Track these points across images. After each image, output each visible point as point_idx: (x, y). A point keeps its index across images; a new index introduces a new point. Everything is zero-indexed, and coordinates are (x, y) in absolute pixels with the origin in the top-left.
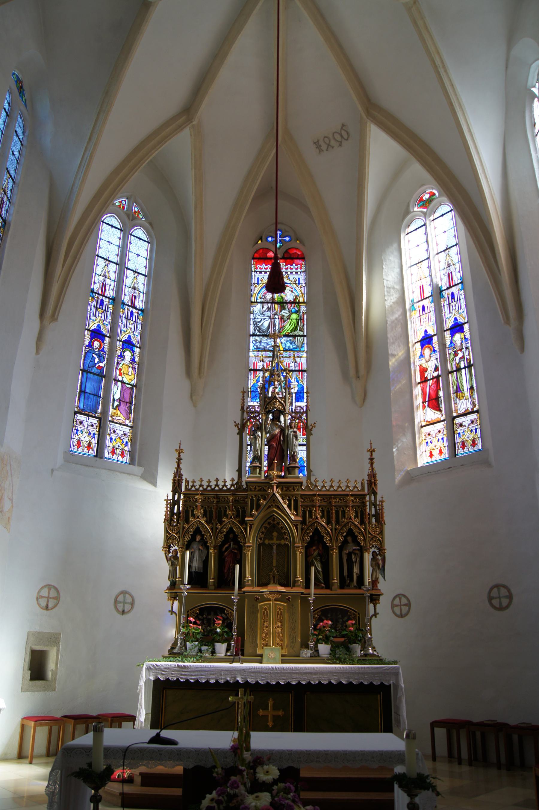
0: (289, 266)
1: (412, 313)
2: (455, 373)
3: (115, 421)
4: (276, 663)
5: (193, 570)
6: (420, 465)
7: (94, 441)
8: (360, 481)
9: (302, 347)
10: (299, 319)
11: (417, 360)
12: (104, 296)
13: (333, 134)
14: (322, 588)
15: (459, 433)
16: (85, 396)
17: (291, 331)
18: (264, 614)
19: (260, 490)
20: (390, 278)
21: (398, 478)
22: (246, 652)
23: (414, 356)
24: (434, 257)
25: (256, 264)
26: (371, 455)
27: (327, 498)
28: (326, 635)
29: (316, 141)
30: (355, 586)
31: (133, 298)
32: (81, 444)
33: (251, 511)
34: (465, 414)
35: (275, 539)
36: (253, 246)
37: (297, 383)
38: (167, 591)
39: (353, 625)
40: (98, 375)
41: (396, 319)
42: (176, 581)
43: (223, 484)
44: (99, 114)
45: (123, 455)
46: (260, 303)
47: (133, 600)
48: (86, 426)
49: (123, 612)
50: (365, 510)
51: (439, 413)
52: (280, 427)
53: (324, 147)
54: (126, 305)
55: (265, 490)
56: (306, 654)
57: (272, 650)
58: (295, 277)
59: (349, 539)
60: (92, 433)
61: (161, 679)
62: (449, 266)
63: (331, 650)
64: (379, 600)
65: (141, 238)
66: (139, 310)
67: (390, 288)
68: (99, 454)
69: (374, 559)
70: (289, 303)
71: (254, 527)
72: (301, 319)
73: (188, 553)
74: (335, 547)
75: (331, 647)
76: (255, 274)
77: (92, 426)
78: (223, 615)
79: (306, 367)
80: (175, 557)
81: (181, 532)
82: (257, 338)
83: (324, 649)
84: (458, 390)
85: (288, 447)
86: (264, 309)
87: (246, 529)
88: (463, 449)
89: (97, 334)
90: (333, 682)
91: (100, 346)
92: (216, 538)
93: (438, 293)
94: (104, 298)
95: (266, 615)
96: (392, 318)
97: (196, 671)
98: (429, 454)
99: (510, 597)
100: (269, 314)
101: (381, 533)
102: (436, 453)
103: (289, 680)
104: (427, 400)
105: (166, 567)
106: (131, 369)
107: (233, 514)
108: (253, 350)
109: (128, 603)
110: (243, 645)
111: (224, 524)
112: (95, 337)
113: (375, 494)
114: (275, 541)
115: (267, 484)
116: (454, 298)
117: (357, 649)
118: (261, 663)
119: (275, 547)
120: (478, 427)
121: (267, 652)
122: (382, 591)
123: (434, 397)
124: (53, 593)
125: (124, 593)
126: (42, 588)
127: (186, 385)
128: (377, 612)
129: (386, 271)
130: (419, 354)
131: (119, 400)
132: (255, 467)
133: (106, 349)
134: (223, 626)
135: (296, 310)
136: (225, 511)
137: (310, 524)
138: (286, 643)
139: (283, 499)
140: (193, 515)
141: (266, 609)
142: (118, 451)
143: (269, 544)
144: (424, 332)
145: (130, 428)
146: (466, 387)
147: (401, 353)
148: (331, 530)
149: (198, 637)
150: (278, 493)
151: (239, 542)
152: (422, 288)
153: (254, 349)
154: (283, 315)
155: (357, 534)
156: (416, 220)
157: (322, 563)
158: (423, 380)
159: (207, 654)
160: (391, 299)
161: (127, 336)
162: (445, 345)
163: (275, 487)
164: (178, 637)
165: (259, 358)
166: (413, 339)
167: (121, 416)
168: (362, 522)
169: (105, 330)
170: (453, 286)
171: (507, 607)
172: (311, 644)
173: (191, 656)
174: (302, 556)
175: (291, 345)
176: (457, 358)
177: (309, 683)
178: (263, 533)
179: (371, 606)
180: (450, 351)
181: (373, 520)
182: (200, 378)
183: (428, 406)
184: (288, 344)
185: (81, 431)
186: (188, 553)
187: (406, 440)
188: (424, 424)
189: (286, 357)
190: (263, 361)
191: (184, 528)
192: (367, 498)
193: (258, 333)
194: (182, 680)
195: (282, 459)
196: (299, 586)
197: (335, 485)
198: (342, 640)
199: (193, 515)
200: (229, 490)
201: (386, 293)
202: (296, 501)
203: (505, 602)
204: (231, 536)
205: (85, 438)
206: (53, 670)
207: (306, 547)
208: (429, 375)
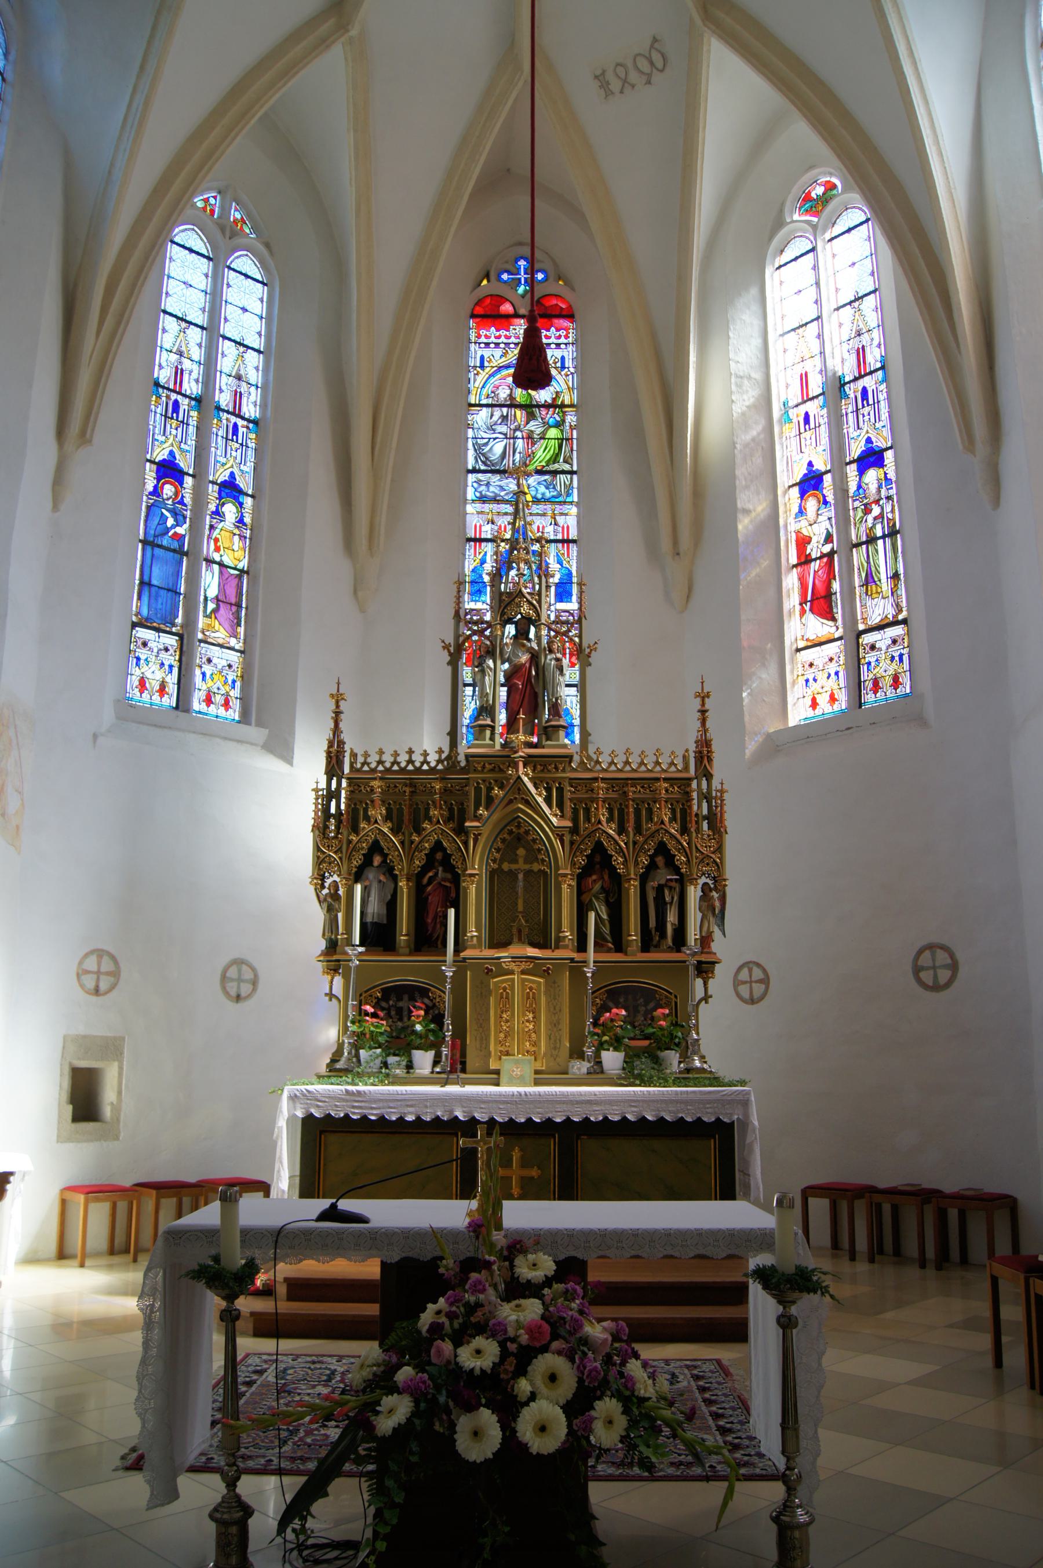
1: (784, 428)
2: (864, 547)
4: (525, 1085)
5: (369, 919)
7: (172, 679)
8: (680, 753)
9: (568, 495)
10: (562, 439)
12: (179, 393)
14: (609, 951)
15: (869, 664)
17: (548, 463)
18: (502, 997)
19: (492, 770)
20: (742, 357)
21: (751, 747)
24: (830, 317)
25: (478, 328)
27: (619, 784)
29: (598, 72)
32: (147, 685)
33: (477, 809)
34: (880, 627)
35: (521, 861)
36: (472, 291)
38: (321, 958)
39: (665, 1016)
40: (174, 551)
41: (753, 440)
42: (337, 939)
43: (422, 759)
44: (159, 12)
45: (226, 705)
46: (487, 406)
47: (256, 976)
48: (155, 650)
49: (238, 998)
50: (690, 807)
51: (831, 623)
52: (530, 650)
53: (615, 85)
54: (224, 411)
55: (501, 771)
56: (579, 1069)
57: (517, 1062)
59: (660, 860)
60: (167, 663)
61: (317, 1115)
63: (625, 1062)
64: (713, 972)
65: (249, 274)
66: (249, 421)
67: (741, 377)
68: (182, 704)
69: (705, 896)
70: (543, 406)
71: (482, 840)
72: (567, 440)
74: (632, 876)
76: (477, 349)
77: (166, 650)
78: (426, 1001)
79: (576, 534)
80: (335, 896)
82: (480, 476)
83: (612, 1059)
84: (870, 580)
85: (544, 688)
86: (495, 418)
87: (466, 844)
89: (168, 470)
90: (630, 1117)
91: (176, 494)
92: (411, 861)
93: (837, 387)
94: (179, 398)
95: (506, 999)
98: (810, 703)
99: (954, 967)
100: (503, 429)
101: (720, 849)
102: (823, 700)
103: (550, 1115)
104: (809, 598)
105: (318, 915)
106: (236, 538)
110: (463, 1054)
111: (424, 833)
112: (165, 476)
113: (709, 776)
114: (521, 865)
115: (505, 759)
117: (672, 1059)
118: (498, 1084)
119: (521, 876)
121: (508, 1066)
124: (107, 965)
125: (239, 962)
126: (87, 955)
129: (735, 342)
130: (795, 509)
131: (217, 599)
132: (483, 727)
133: (188, 500)
136: (427, 810)
139: (536, 787)
140: (367, 818)
141: (505, 989)
142: (219, 699)
145: (239, 654)
147: (760, 508)
149: (381, 1039)
150: (527, 775)
151: (453, 867)
152: (804, 379)
153: (475, 498)
155: (674, 852)
157: (608, 904)
159: (398, 1071)
160: (744, 400)
161: (227, 473)
163: (521, 765)
165: (484, 517)
166: (785, 479)
167: (222, 629)
168: (684, 830)
169: (185, 463)
170: (866, 374)
171: (948, 984)
172: (589, 1052)
173: (370, 1075)
176: (870, 518)
177: (587, 1119)
178: (498, 850)
179: (699, 982)
181: (705, 825)
183: (811, 610)
184: (542, 489)
185: (146, 660)
186: (358, 888)
187: (766, 676)
188: (801, 644)
189: (538, 514)
190: (493, 523)
191: (350, 842)
193: (483, 467)
194: (355, 1117)
195: (534, 710)
196: (566, 947)
197: (635, 761)
199: (367, 818)
201: (734, 387)
202: (560, 790)
203: (944, 975)
204: (439, 856)
205: (154, 675)
206: (112, 1103)
208: (815, 550)
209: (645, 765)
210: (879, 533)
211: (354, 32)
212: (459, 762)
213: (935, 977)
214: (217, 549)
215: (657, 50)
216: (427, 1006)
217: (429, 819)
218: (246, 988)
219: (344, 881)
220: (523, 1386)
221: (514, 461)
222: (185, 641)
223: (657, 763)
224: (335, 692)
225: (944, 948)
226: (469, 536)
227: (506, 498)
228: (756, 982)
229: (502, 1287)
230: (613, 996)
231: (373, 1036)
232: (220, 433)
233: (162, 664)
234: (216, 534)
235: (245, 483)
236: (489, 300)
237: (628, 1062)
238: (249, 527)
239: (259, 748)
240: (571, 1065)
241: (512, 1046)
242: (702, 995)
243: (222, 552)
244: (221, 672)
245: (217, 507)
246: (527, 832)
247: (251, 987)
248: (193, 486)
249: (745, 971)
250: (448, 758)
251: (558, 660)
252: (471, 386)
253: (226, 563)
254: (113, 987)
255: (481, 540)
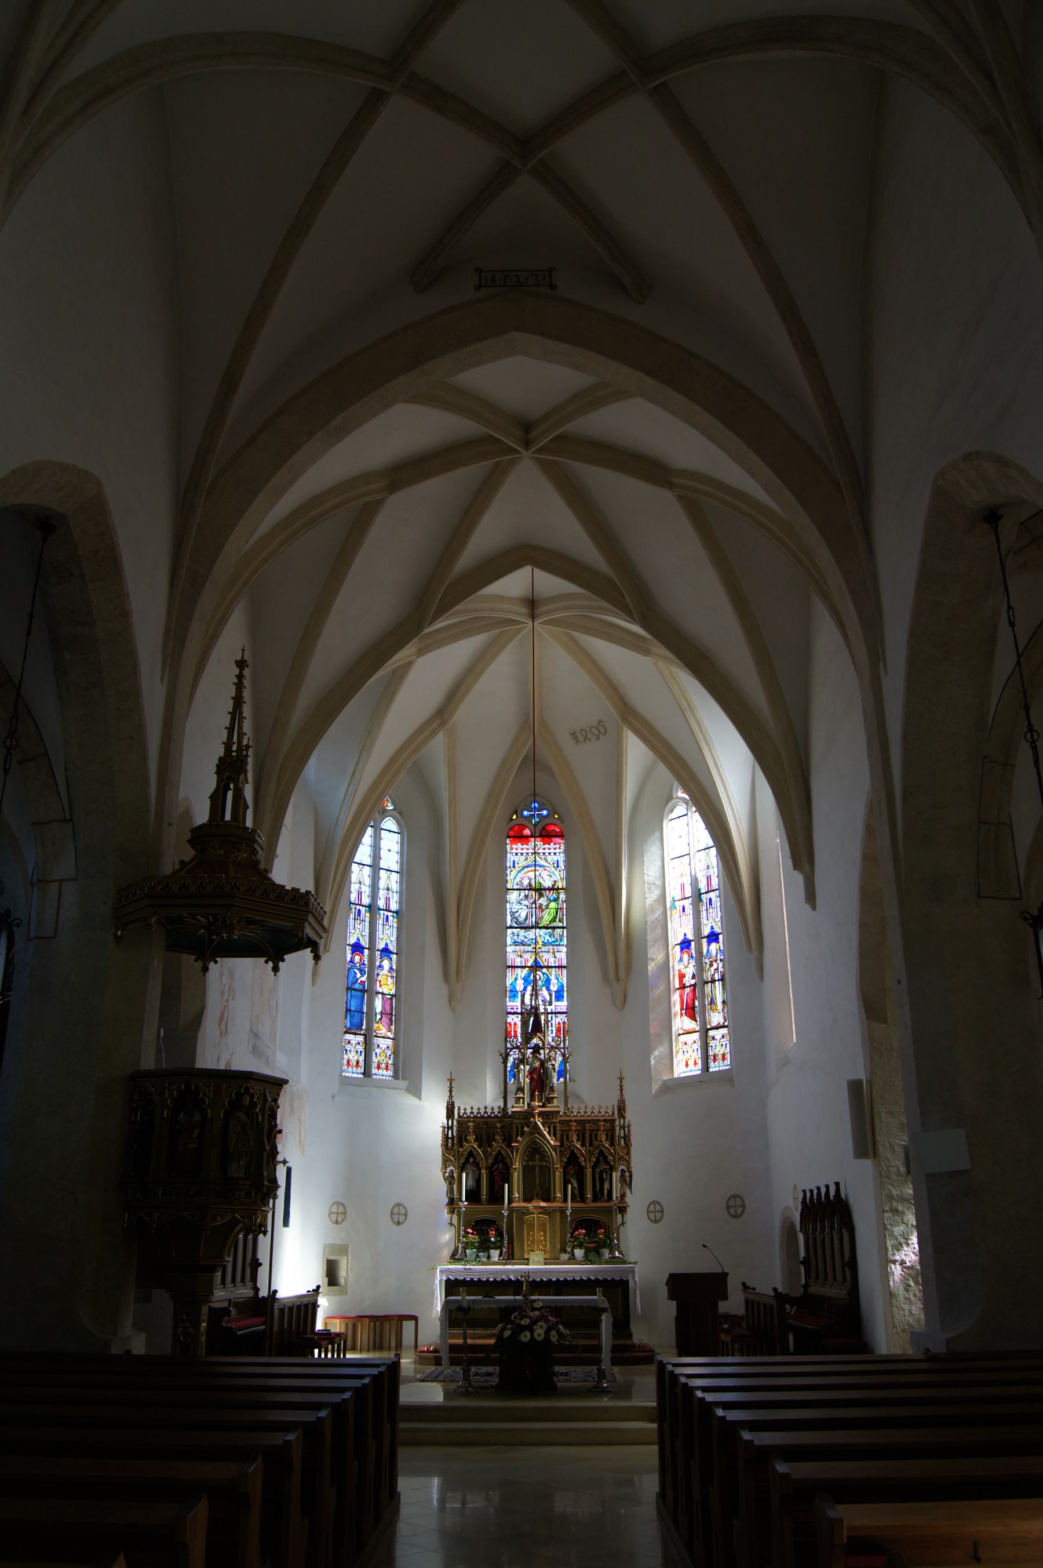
0: (547, 846)
1: (673, 912)
2: (710, 984)
3: (378, 1035)
4: (540, 1265)
5: (468, 1188)
6: (676, 1076)
7: (362, 1059)
8: (610, 1107)
9: (561, 940)
10: (558, 909)
11: (676, 963)
12: (361, 905)
13: (590, 728)
14: (578, 1202)
15: (712, 1046)
16: (350, 1014)
17: (550, 923)
18: (529, 1225)
20: (651, 872)
21: (655, 1087)
22: (515, 1257)
23: (673, 959)
24: (694, 856)
25: (512, 843)
26: (621, 1082)
27: (581, 1123)
28: (581, 1242)
29: (572, 732)
30: (605, 1200)
31: (388, 900)
32: (351, 1063)
33: (517, 1137)
34: (717, 1028)
35: (537, 1161)
36: (508, 824)
37: (557, 981)
38: (447, 1207)
39: (602, 1233)
40: (361, 991)
41: (656, 919)
42: (454, 1198)
43: (491, 1111)
44: (362, 751)
47: (406, 1211)
48: (354, 1044)
49: (399, 1223)
50: (615, 1133)
51: (694, 1022)
52: (540, 1060)
53: (581, 739)
54: (381, 910)
56: (564, 1258)
58: (554, 859)
59: (601, 1159)
60: (359, 1051)
61: (452, 1279)
62: (708, 867)
63: (585, 1254)
64: (626, 1212)
65: (391, 830)
66: (393, 912)
67: (650, 884)
68: (367, 1073)
69: (622, 1176)
70: (547, 889)
71: (520, 1151)
72: (560, 909)
73: (464, 1175)
74: (588, 1167)
75: (585, 1251)
76: (511, 856)
77: (359, 1043)
78: (495, 1226)
79: (566, 962)
80: (452, 1177)
81: (456, 1154)
82: (514, 930)
83: (579, 1253)
84: (712, 1002)
85: (547, 1079)
86: (522, 897)
88: (714, 1062)
89: (357, 948)
90: (584, 1278)
91: (361, 960)
92: (487, 1159)
94: (361, 907)
95: (531, 1227)
96: (651, 918)
97: (478, 1272)
98: (685, 1064)
99: (743, 1206)
100: (526, 903)
101: (628, 1153)
102: (691, 1063)
103: (551, 1278)
104: (684, 1008)
105: (444, 1186)
106: (389, 978)
107: (501, 1139)
108: (510, 945)
109: (402, 1214)
110: (513, 1251)
111: (493, 1147)
113: (624, 1118)
114: (537, 1163)
115: (528, 1114)
116: (711, 905)
117: (606, 1253)
118: (528, 1265)
119: (537, 1168)
120: (728, 1042)
122: (629, 1204)
123: (691, 1006)
124: (341, 1209)
125: (398, 1205)
126: (332, 1205)
127: (444, 989)
128: (625, 1221)
129: (647, 864)
130: (678, 958)
131: (381, 1013)
132: (519, 1098)
133: (366, 962)
134: (496, 1236)
135: (555, 898)
137: (567, 1147)
138: (548, 1248)
139: (544, 1127)
140: (467, 1140)
141: (531, 1221)
142: (383, 1066)
143: (532, 1166)
144: (683, 935)
145: (392, 1041)
146: (719, 1000)
147: (660, 957)
148: (586, 1151)
149: (476, 1245)
150: (539, 1121)
151: (506, 1163)
152: (683, 886)
153: (511, 943)
154: (541, 904)
155: (607, 1155)
156: (679, 806)
158: (682, 986)
159: (484, 1259)
160: (652, 897)
161: (384, 944)
162: (702, 953)
163: (537, 1116)
164: (458, 1246)
165: (516, 954)
166: (673, 940)
167: (384, 1029)
168: (612, 1144)
169: (365, 943)
170: (711, 891)
171: (741, 1215)
173: (472, 1261)
174: (561, 1174)
175: (550, 938)
176: (713, 969)
177: (566, 1279)
178: (527, 1156)
179: (619, 1216)
180: (707, 960)
182: (458, 982)
183: (686, 1014)
184: (547, 937)
185: (350, 1050)
186: (464, 1175)
188: (681, 1032)
189: (545, 952)
190: (521, 957)
191: (459, 1151)
192: (617, 1123)
193: (515, 925)
194: (468, 1279)
195: (542, 1090)
196: (557, 1201)
198: (594, 1245)
199: (467, 1140)
200: (496, 1117)
201: (646, 889)
202: (555, 1128)
203: (739, 1210)
205: (353, 1057)
206: (344, 1277)
207: (564, 1166)
208: (687, 982)
209: (594, 1113)
210: (717, 978)
211: (449, 726)
212: (508, 1113)
213: (736, 1211)
214: (381, 986)
215: (601, 725)
216: (495, 1228)
217: (495, 1140)
218: (402, 1218)
219: (457, 1170)
220: (535, 1327)
221: (532, 922)
222: (367, 1038)
223: (600, 1112)
224: (450, 1078)
225: (739, 1197)
226: (508, 964)
227: (528, 942)
228: (657, 1211)
229: (530, 1309)
230: (580, 1224)
231: (472, 1243)
232: (380, 923)
233: (357, 1052)
234: (379, 978)
235: (392, 948)
236: (517, 828)
237: (586, 1255)
238: (395, 970)
239: (404, 1091)
240: (560, 1255)
241: (534, 1247)
242: (621, 1222)
243: (383, 987)
244: (384, 1051)
245: (380, 963)
246: (540, 1147)
247: (404, 1217)
248: (369, 954)
249: (652, 1206)
250: (503, 1110)
251: (553, 1065)
252: (508, 878)
253: (385, 993)
254: (343, 1220)
255: (515, 967)
